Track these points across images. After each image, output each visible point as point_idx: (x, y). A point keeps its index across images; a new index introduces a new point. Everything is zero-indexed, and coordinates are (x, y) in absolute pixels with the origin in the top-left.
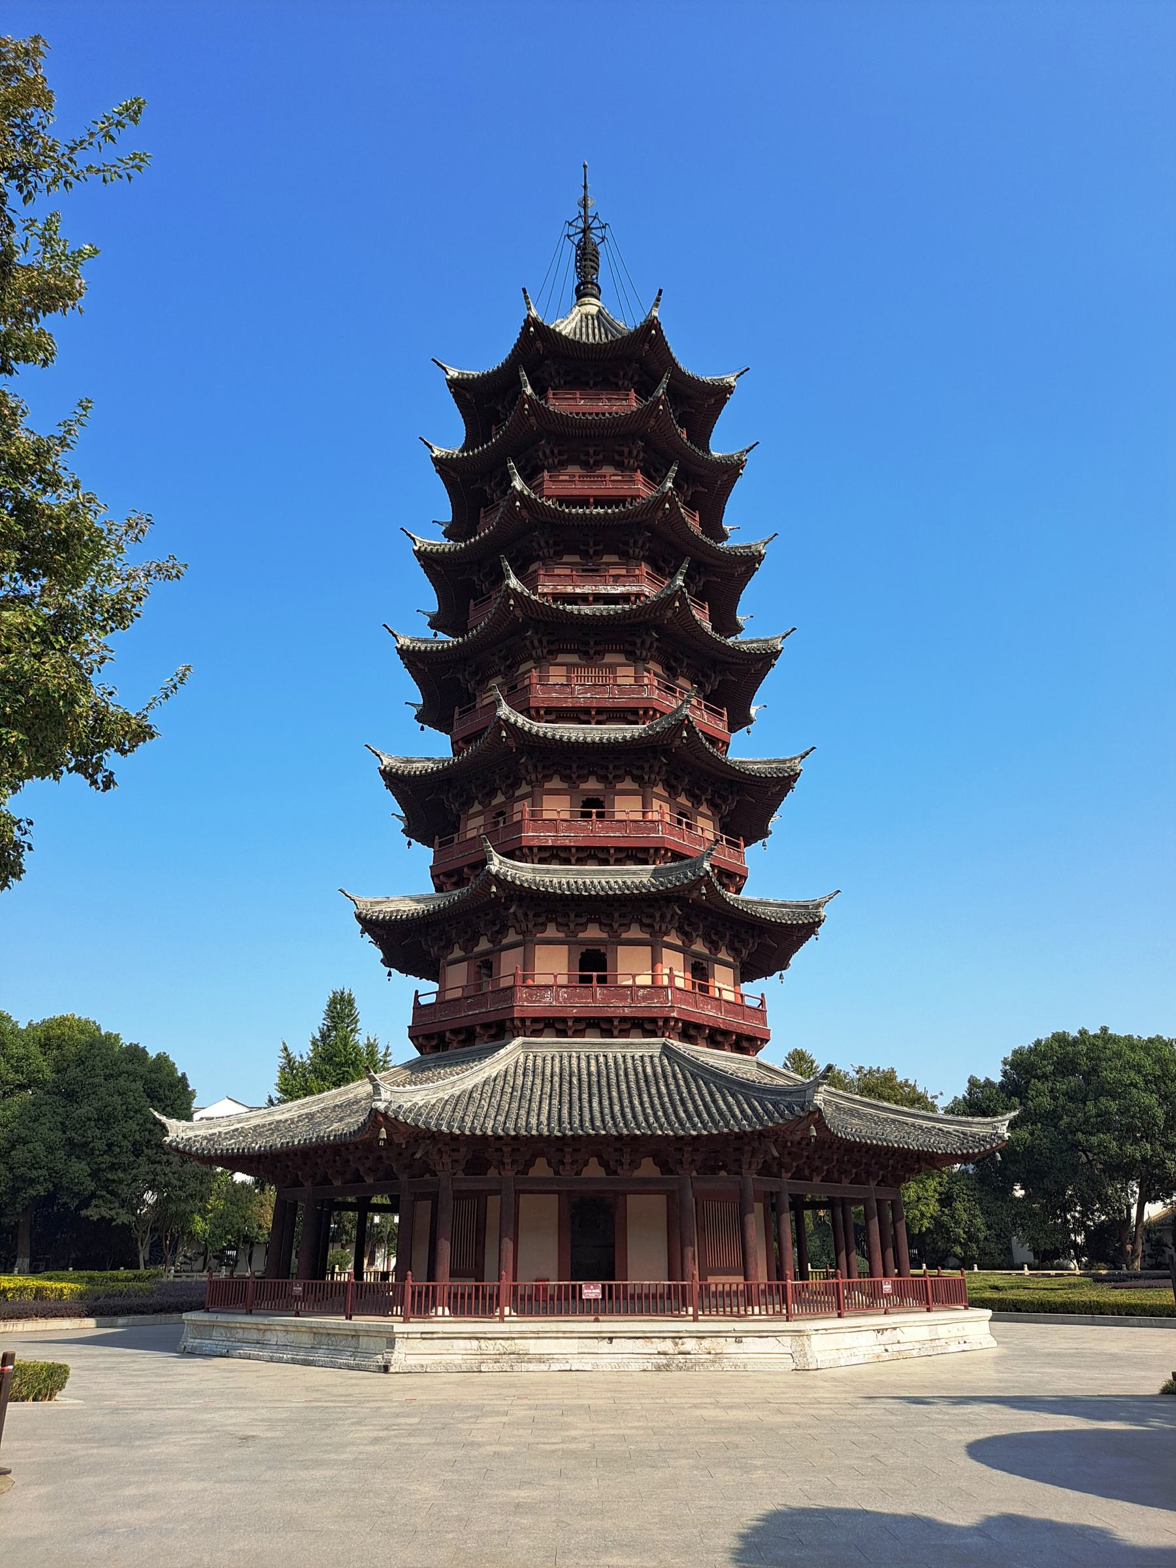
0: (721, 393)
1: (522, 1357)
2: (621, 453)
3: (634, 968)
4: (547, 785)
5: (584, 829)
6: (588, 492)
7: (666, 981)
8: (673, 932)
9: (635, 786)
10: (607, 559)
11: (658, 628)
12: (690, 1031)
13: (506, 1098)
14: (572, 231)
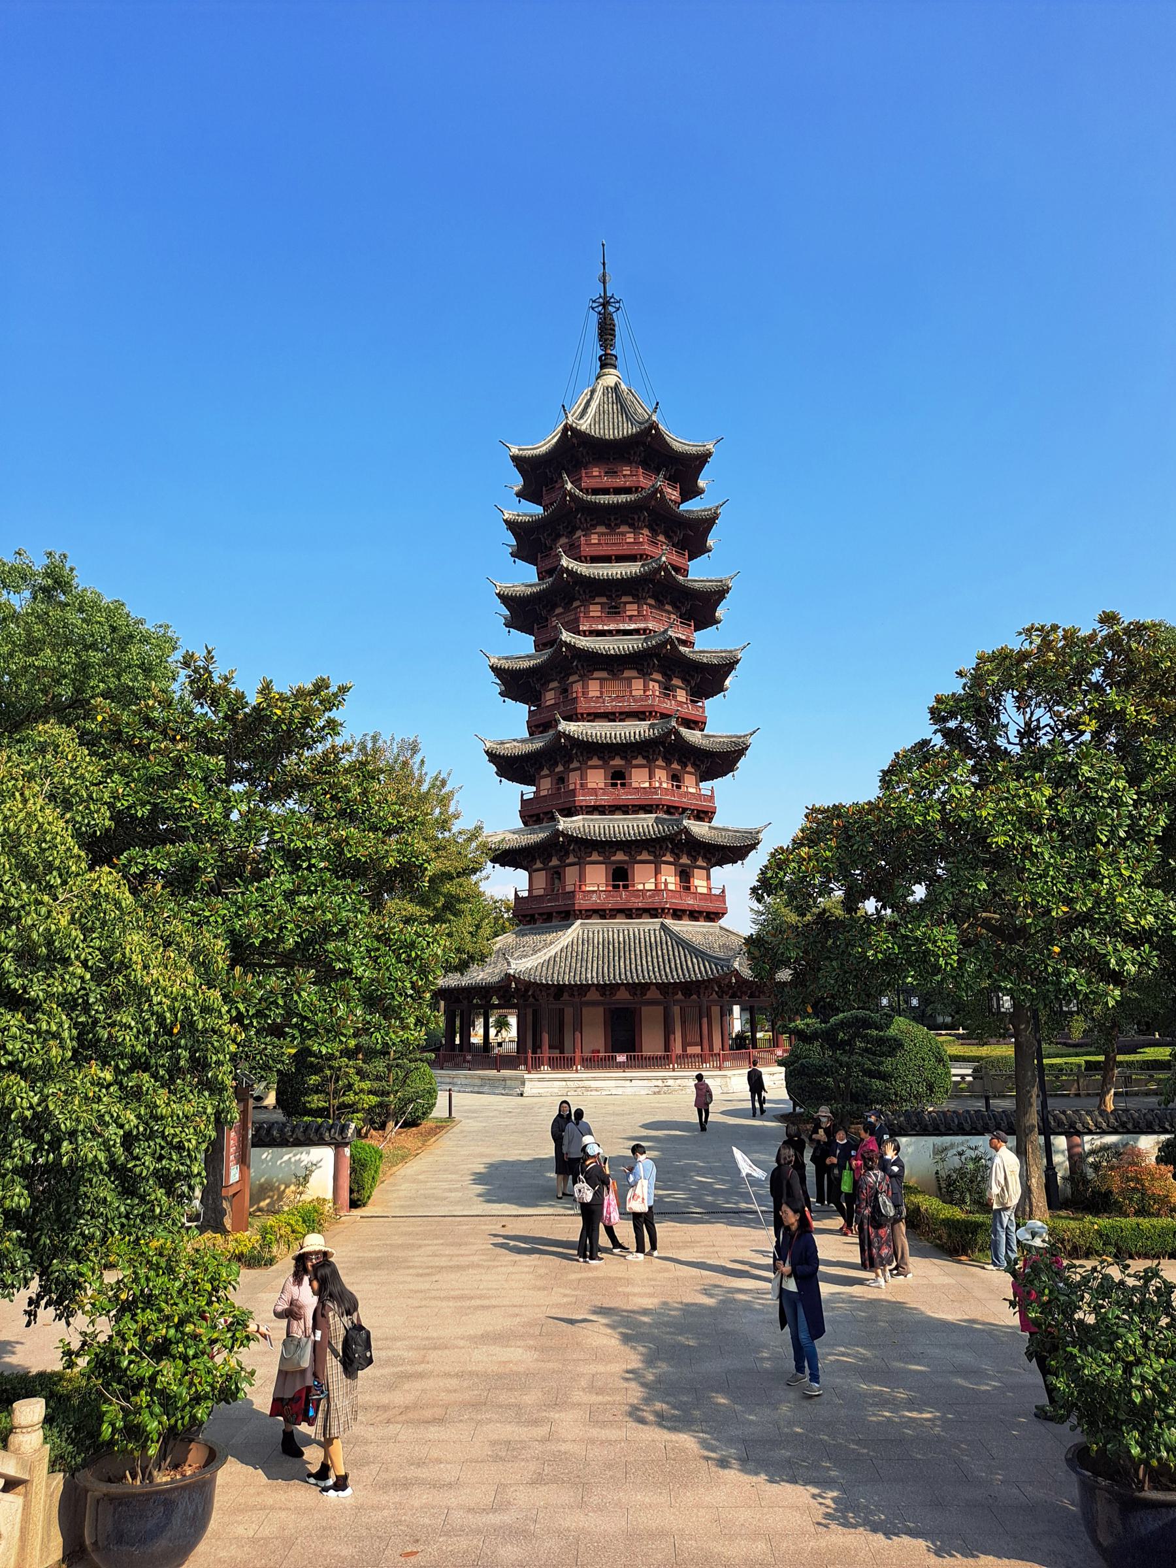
0: (702, 459)
1: (588, 1089)
2: (633, 519)
3: (644, 880)
4: (590, 763)
5: (612, 794)
6: (611, 553)
7: (657, 785)
8: (668, 854)
9: (644, 762)
10: (624, 599)
11: (647, 509)
12: (678, 914)
13: (574, 960)
14: (595, 305)
